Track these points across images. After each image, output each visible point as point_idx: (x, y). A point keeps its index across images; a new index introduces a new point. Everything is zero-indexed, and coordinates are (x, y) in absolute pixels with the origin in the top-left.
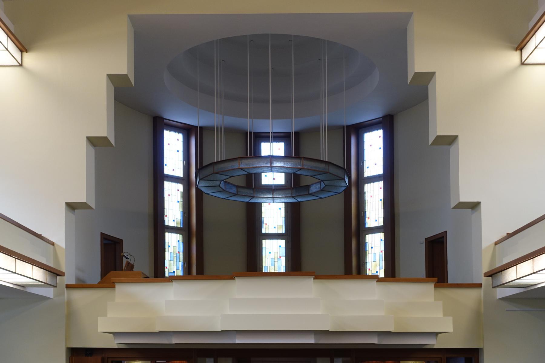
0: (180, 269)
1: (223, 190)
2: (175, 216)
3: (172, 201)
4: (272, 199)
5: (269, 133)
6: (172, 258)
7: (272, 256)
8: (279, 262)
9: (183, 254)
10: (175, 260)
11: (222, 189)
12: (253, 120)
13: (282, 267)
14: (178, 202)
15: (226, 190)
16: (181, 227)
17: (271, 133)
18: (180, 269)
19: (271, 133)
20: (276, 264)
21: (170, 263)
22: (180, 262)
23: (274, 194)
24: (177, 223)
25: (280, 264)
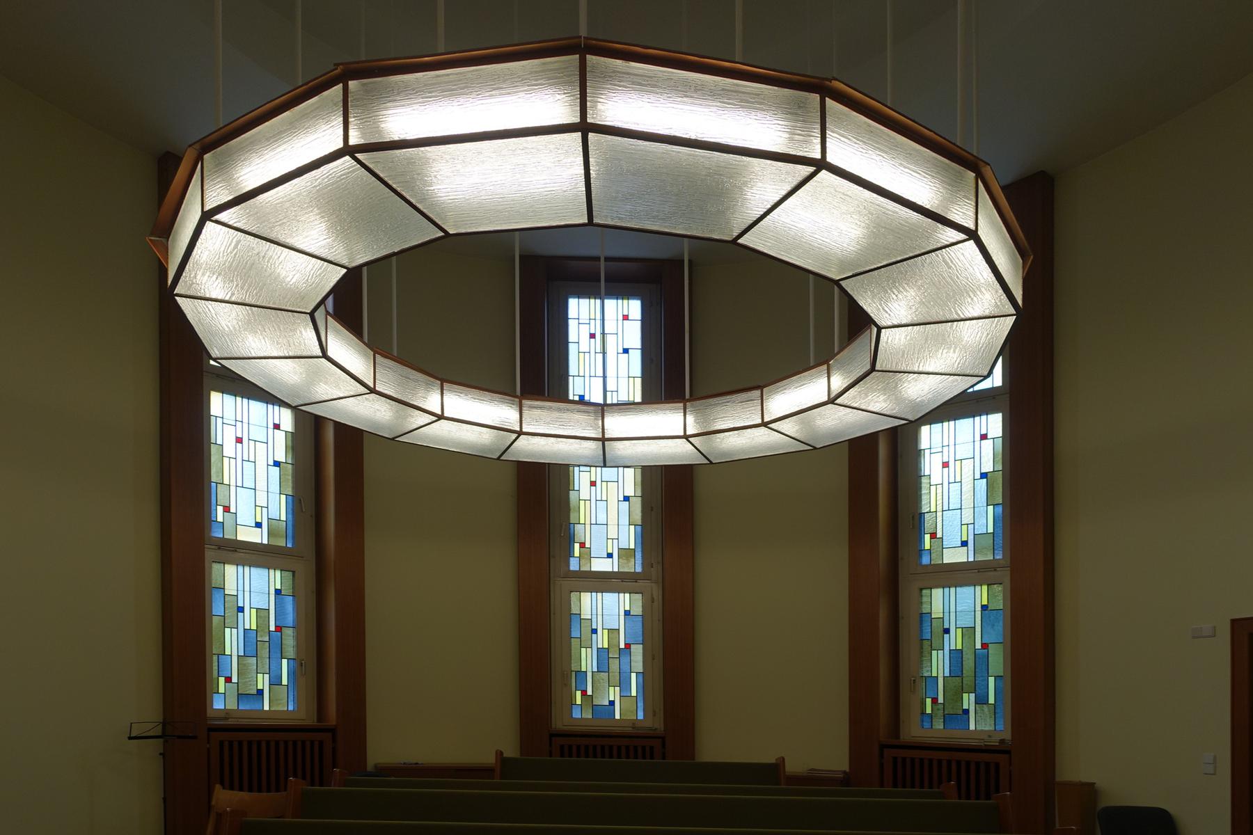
0: (285, 681)
1: (435, 418)
2: (265, 510)
3: (252, 459)
4: (607, 436)
5: (598, 259)
6: (251, 650)
7: (602, 640)
8: (625, 659)
9: (295, 634)
10: (264, 653)
11: (431, 417)
12: (611, 570)
13: (634, 676)
14: (277, 464)
15: (524, 430)
16: (289, 545)
17: (602, 260)
18: (285, 681)
19: (602, 260)
20: (614, 665)
21: (245, 665)
22: (285, 662)
23: (291, 662)
24: (270, 534)
25: (625, 668)
